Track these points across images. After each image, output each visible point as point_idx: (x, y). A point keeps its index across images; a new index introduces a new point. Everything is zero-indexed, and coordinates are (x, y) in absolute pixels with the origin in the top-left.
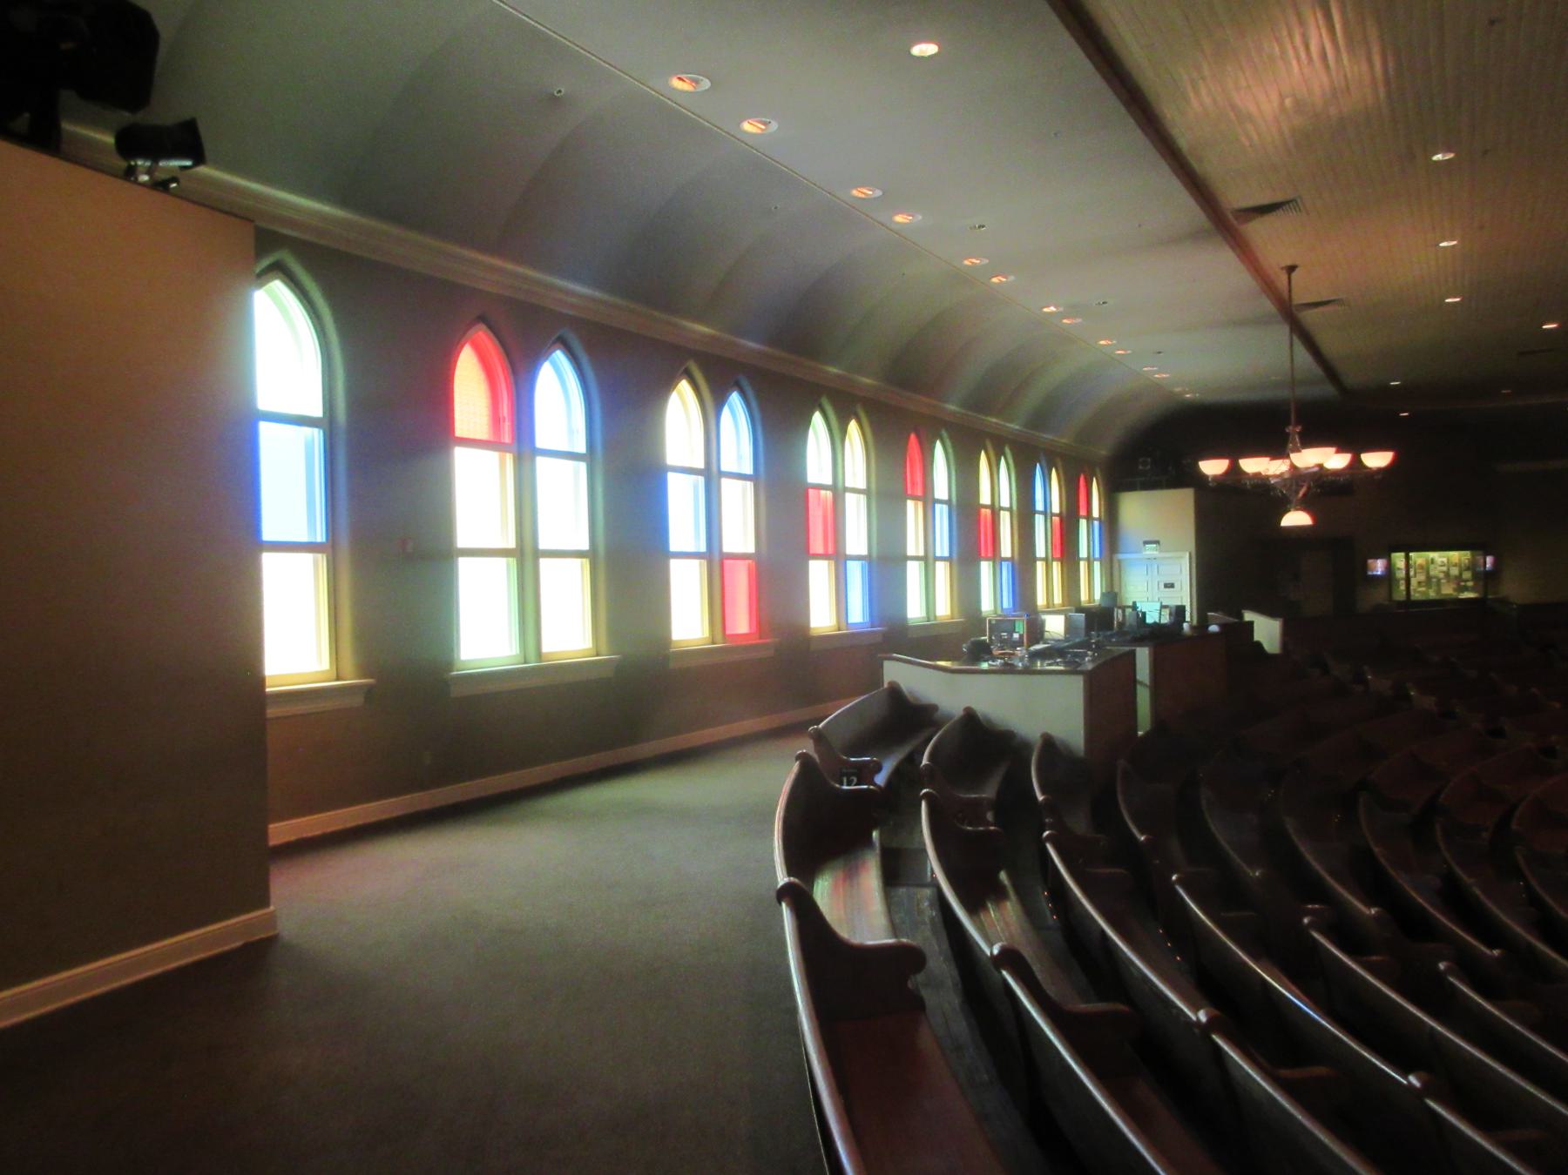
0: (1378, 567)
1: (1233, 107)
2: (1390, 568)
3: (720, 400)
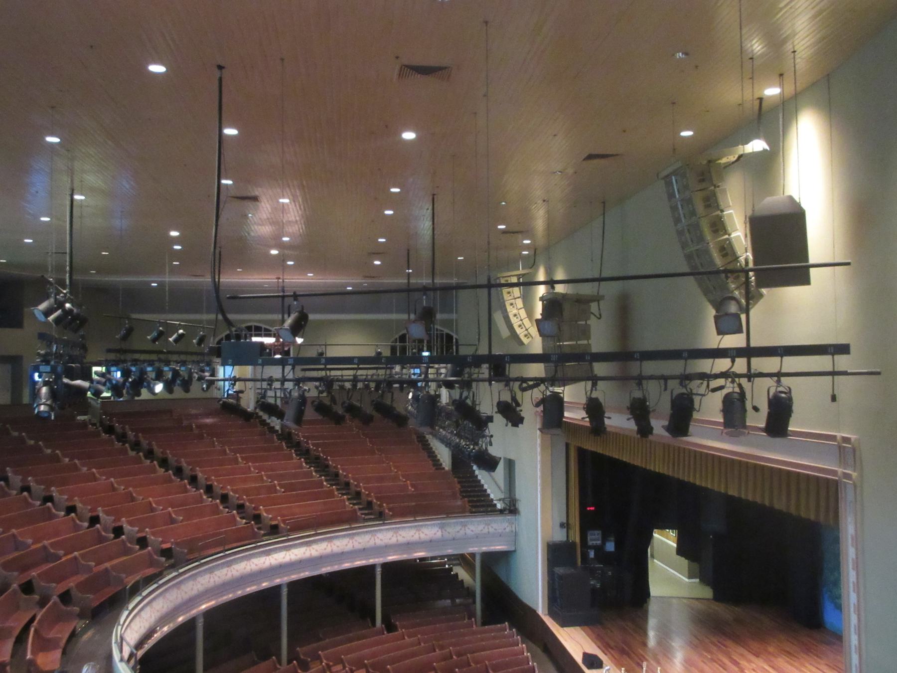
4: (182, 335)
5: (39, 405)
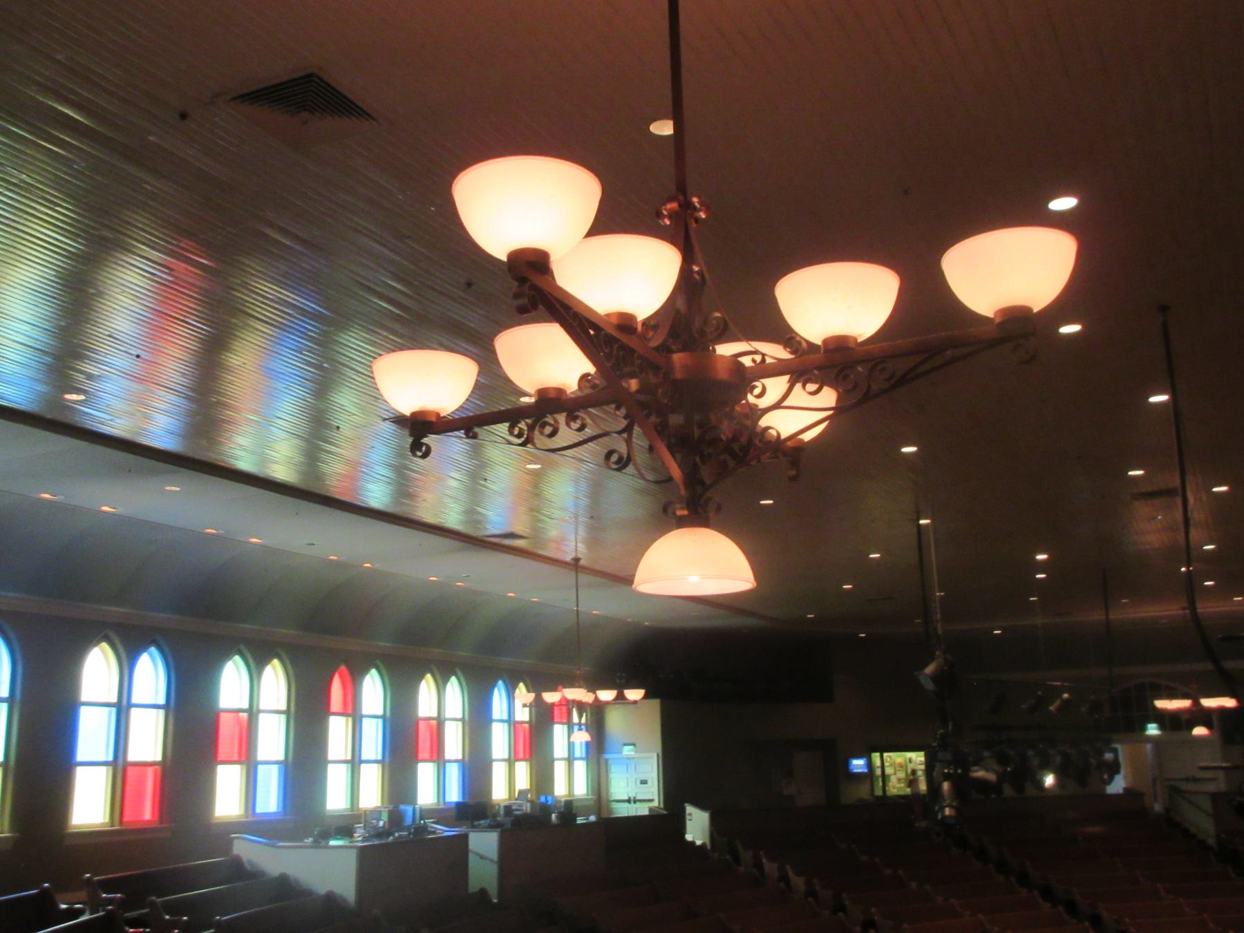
0: (858, 764)
1: (285, 259)
2: (870, 765)
3: (446, 680)
4: (1066, 702)
5: (942, 808)
